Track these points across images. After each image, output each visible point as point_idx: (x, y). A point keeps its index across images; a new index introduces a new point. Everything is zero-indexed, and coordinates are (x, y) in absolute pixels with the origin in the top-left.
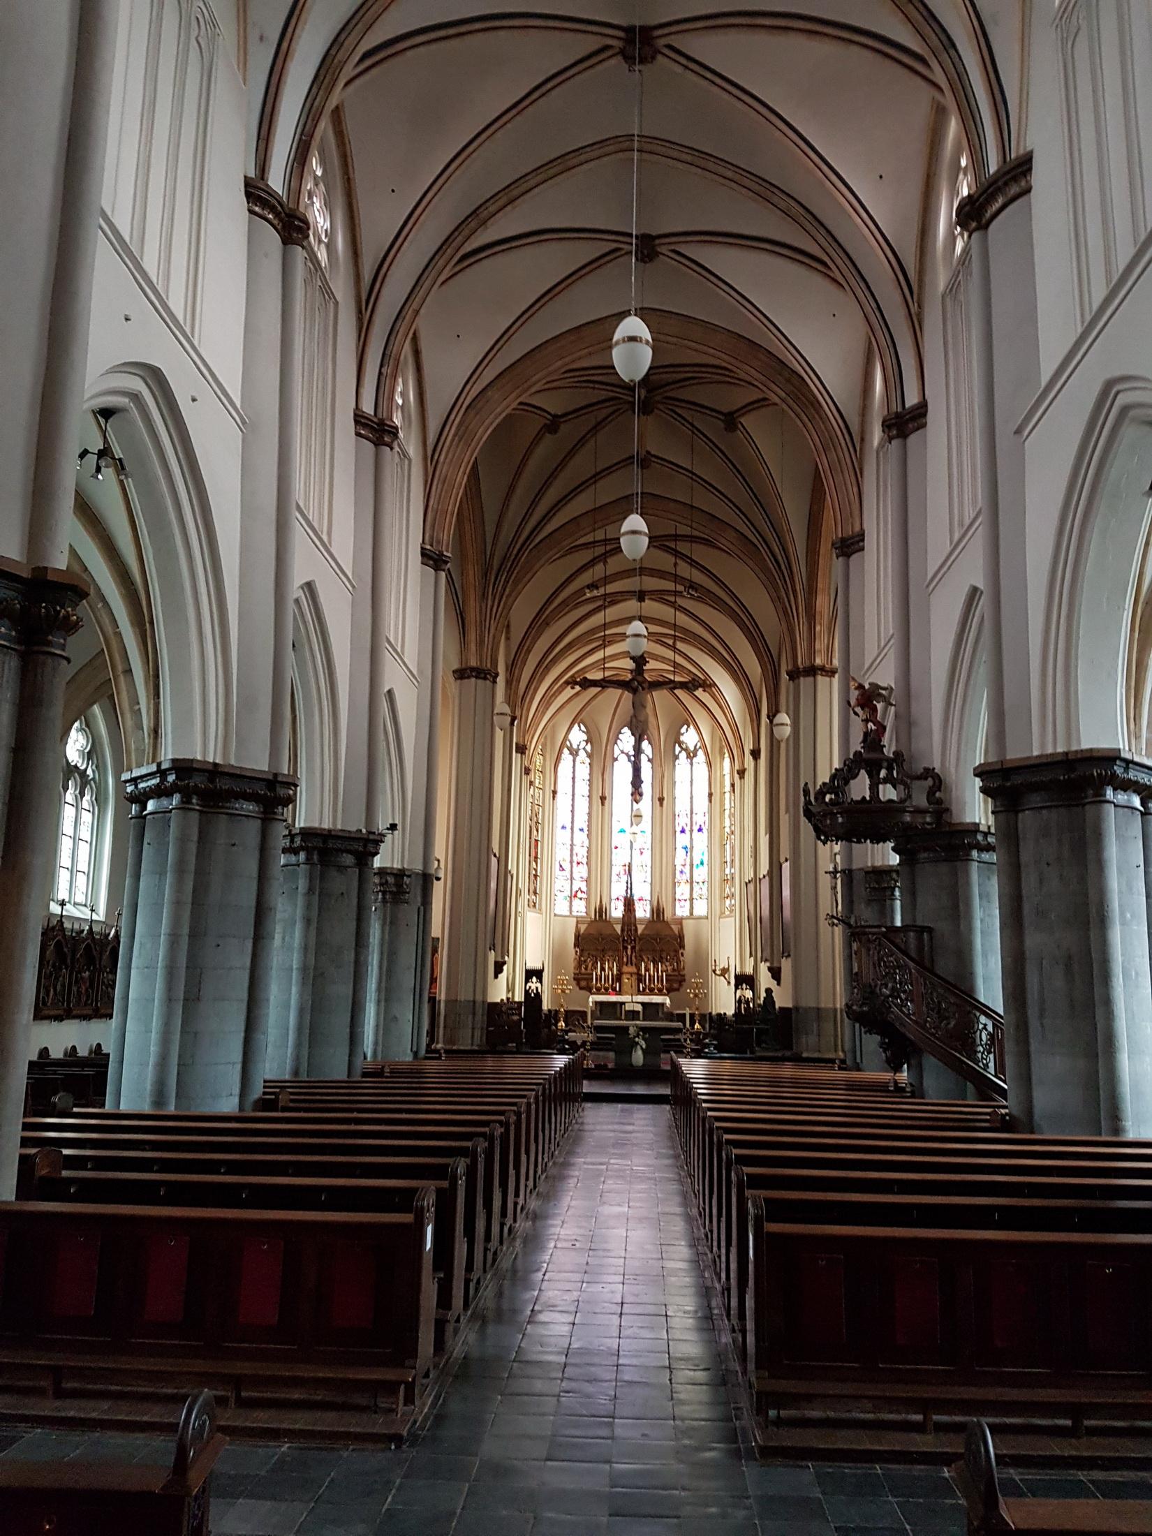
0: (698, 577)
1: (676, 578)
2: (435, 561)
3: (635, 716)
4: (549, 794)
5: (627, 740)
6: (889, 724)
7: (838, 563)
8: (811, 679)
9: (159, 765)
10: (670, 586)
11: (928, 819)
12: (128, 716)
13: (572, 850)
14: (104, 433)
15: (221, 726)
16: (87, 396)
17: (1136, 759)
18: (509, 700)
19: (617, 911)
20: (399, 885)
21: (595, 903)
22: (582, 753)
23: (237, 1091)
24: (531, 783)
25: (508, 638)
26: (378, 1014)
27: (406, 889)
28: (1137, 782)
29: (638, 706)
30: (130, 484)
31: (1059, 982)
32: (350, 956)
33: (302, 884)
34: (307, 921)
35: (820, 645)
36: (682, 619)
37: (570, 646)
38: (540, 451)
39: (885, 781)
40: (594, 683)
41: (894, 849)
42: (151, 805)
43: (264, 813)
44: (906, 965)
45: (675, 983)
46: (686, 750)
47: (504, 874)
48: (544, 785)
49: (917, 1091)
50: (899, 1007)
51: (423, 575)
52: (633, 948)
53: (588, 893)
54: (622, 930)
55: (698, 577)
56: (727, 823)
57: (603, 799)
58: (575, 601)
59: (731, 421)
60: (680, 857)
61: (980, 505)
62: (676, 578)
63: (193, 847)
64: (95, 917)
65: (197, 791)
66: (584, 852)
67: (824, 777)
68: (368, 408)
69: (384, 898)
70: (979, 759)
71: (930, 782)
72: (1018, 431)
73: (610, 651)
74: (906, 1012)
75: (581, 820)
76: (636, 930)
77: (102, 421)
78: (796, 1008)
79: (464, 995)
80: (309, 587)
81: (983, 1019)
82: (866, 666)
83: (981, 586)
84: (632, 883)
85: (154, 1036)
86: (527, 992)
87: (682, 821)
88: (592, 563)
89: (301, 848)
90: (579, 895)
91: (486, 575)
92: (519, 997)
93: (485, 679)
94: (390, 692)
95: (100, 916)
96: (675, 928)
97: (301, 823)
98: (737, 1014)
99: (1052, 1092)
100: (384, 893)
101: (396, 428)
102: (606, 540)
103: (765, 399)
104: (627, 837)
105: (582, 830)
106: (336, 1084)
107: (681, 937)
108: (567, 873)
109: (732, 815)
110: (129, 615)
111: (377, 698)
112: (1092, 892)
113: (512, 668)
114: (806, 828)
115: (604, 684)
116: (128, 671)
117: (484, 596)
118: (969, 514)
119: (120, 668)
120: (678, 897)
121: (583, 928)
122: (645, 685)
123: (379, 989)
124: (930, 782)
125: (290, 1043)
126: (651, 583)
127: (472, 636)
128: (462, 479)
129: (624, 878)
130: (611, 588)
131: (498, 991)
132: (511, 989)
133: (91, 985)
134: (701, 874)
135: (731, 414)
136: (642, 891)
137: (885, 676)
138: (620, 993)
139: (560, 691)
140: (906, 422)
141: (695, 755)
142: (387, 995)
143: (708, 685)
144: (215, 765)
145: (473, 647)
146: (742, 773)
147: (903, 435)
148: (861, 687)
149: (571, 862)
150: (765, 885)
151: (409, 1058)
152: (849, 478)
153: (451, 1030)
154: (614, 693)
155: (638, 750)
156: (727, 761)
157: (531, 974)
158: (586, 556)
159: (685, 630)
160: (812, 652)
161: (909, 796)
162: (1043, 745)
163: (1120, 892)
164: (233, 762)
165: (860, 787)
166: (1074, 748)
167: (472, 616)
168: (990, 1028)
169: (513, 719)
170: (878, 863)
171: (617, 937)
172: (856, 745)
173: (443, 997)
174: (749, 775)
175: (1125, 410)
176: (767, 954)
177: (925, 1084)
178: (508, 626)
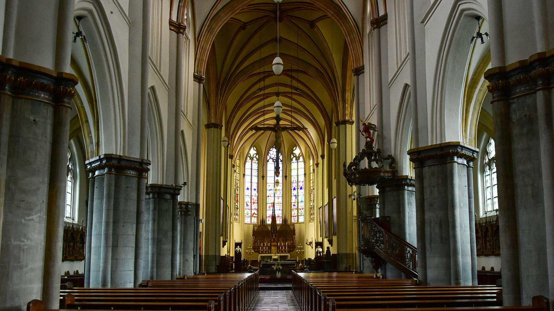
0: (300, 86)
1: (292, 87)
2: (199, 79)
3: (276, 141)
4: (242, 175)
5: (273, 152)
6: (375, 139)
7: (354, 78)
8: (344, 126)
9: (100, 157)
10: (289, 90)
11: (390, 175)
12: (87, 139)
13: (251, 198)
14: (78, 27)
15: (122, 141)
16: (76, 8)
17: (466, 146)
18: (227, 134)
19: (269, 221)
20: (187, 208)
21: (260, 218)
22: (255, 159)
23: (133, 281)
24: (235, 171)
25: (226, 112)
26: (180, 258)
27: (189, 210)
28: (465, 155)
29: (277, 137)
30: (87, 45)
31: (437, 230)
32: (170, 234)
33: (151, 206)
34: (154, 220)
35: (348, 112)
36: (295, 104)
37: (250, 115)
38: (239, 36)
39: (374, 160)
40: (261, 129)
41: (377, 187)
42: (97, 173)
43: (139, 175)
44: (381, 230)
45: (292, 248)
46: (296, 157)
47: (226, 206)
48: (240, 171)
49: (384, 277)
50: (378, 246)
51: (194, 85)
52: (275, 236)
53: (258, 214)
54: (271, 229)
55: (300, 86)
56: (312, 185)
57: (263, 177)
58: (250, 98)
59: (312, 24)
60: (293, 198)
61: (408, 51)
62: (292, 87)
63: (113, 188)
64: (74, 222)
65: (113, 166)
66: (256, 198)
67: (349, 161)
68: (174, 19)
69: (181, 214)
70: (408, 148)
71: (390, 160)
72: (422, 22)
73: (266, 117)
74: (381, 249)
75: (255, 186)
76: (277, 228)
77: (77, 21)
78: (338, 254)
79: (212, 253)
80: (153, 88)
81: (408, 249)
82: (366, 117)
83: (409, 83)
84: (275, 210)
85: (102, 261)
86: (235, 251)
87: (294, 185)
88: (259, 81)
89: (151, 192)
90: (254, 215)
91: (217, 86)
92: (232, 254)
93: (217, 128)
94: (182, 131)
95: (76, 221)
96: (292, 227)
97: (150, 182)
98: (317, 257)
99: (434, 273)
100: (181, 212)
101: (185, 26)
102: (264, 72)
103: (326, 15)
104: (272, 192)
105: (255, 190)
106: (169, 281)
107: (294, 230)
108: (249, 207)
109: (313, 182)
110: (87, 99)
111: (178, 134)
112: (449, 196)
113: (228, 124)
114: (343, 179)
115: (265, 129)
116: (87, 121)
117: (217, 95)
118: (404, 56)
119: (84, 120)
120: (293, 215)
121: (256, 228)
122: (281, 129)
123: (180, 249)
124: (390, 160)
125: (149, 267)
126: (282, 89)
127: (213, 111)
128: (209, 47)
129: (272, 208)
130: (267, 91)
131: (224, 252)
132: (229, 252)
133: (74, 248)
134: (301, 205)
135: (313, 21)
136: (278, 213)
137: (374, 121)
138: (271, 253)
139: (247, 132)
140: (380, 22)
141: (299, 159)
142: (184, 251)
143: (304, 129)
144: (120, 156)
145: (213, 116)
146: (317, 165)
147: (379, 27)
148: (364, 124)
149: (251, 202)
150: (327, 208)
151: (193, 275)
152: (358, 46)
153: (207, 266)
154: (268, 133)
155: (278, 157)
156: (311, 161)
157: (238, 245)
158: (257, 78)
159: (295, 108)
160: (344, 115)
161: (383, 166)
162: (432, 141)
163: (459, 196)
164: (126, 155)
165: (365, 164)
166: (443, 142)
167: (212, 103)
168: (411, 252)
169: (229, 144)
170: (370, 195)
171: (268, 231)
172: (363, 147)
173: (204, 254)
174: (320, 166)
175: (463, 11)
176: (327, 235)
177: (387, 274)
178: (226, 107)
